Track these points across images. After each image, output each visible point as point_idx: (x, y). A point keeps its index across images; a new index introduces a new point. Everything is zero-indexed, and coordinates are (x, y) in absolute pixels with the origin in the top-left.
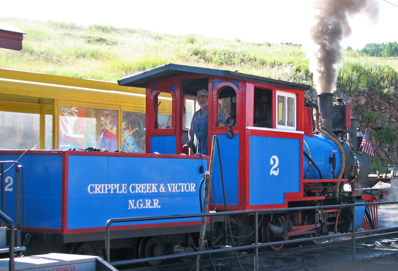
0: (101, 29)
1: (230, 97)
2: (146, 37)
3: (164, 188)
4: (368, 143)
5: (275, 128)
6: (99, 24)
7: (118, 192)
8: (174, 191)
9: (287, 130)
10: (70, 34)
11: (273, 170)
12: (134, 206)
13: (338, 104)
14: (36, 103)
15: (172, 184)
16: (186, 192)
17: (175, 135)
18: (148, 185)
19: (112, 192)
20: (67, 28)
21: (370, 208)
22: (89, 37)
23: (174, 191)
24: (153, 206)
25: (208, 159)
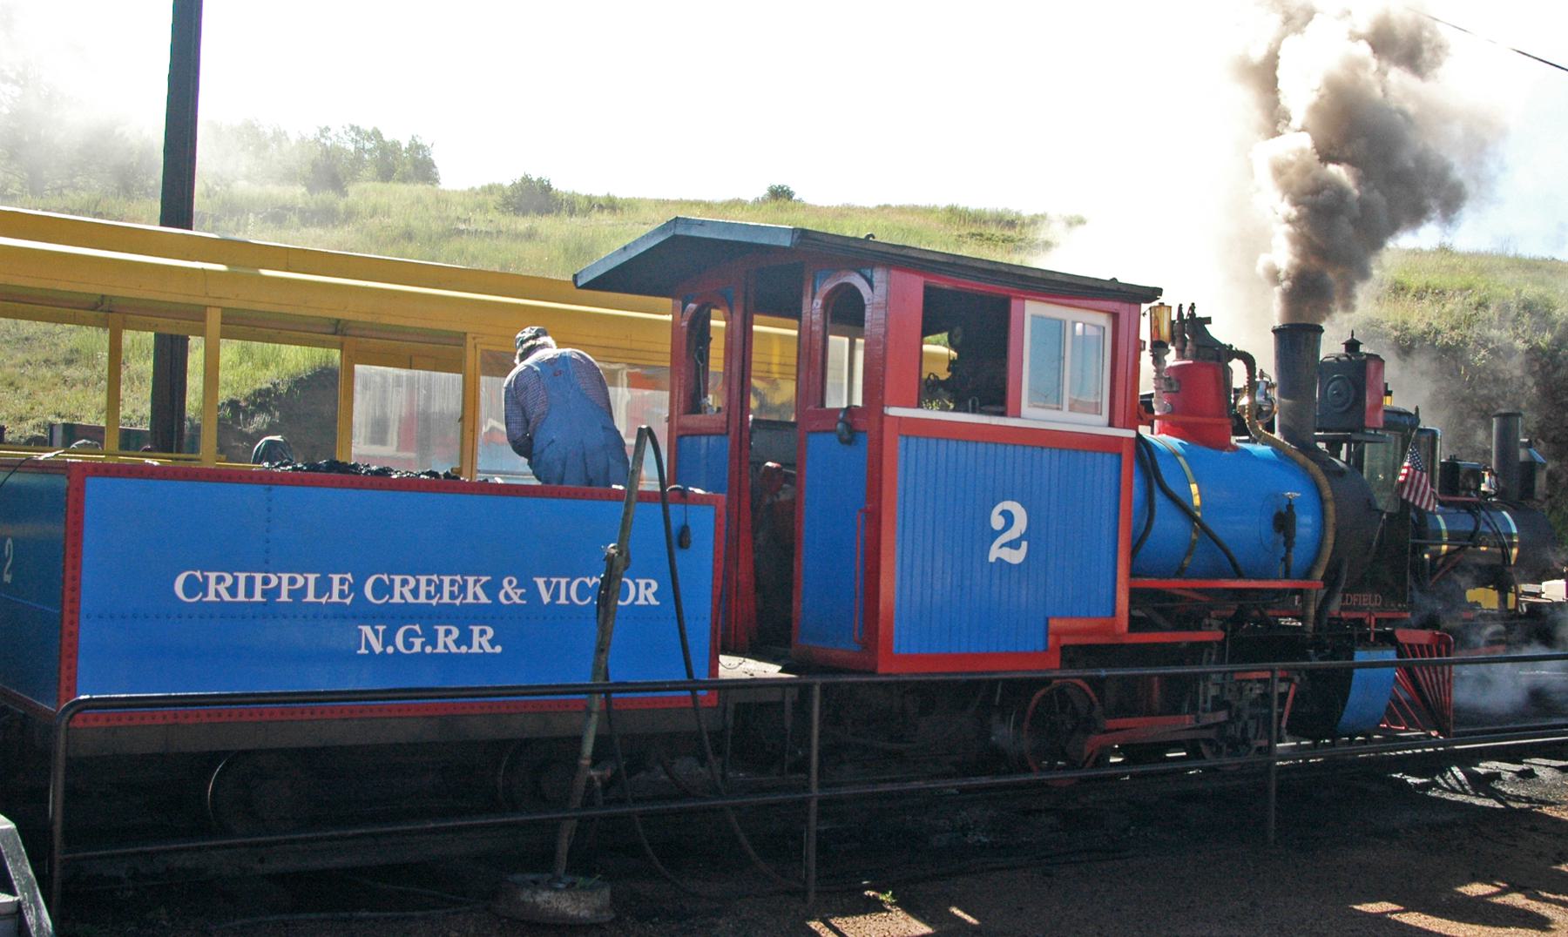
1: (946, 330)
3: (519, 591)
4: (1418, 473)
5: (1018, 415)
7: (310, 597)
10: (981, 235)
12: (385, 646)
14: (85, 309)
15: (554, 580)
16: (576, 605)
17: (727, 433)
18: (447, 580)
19: (284, 597)
20: (985, 222)
23: (563, 600)
24: (470, 647)
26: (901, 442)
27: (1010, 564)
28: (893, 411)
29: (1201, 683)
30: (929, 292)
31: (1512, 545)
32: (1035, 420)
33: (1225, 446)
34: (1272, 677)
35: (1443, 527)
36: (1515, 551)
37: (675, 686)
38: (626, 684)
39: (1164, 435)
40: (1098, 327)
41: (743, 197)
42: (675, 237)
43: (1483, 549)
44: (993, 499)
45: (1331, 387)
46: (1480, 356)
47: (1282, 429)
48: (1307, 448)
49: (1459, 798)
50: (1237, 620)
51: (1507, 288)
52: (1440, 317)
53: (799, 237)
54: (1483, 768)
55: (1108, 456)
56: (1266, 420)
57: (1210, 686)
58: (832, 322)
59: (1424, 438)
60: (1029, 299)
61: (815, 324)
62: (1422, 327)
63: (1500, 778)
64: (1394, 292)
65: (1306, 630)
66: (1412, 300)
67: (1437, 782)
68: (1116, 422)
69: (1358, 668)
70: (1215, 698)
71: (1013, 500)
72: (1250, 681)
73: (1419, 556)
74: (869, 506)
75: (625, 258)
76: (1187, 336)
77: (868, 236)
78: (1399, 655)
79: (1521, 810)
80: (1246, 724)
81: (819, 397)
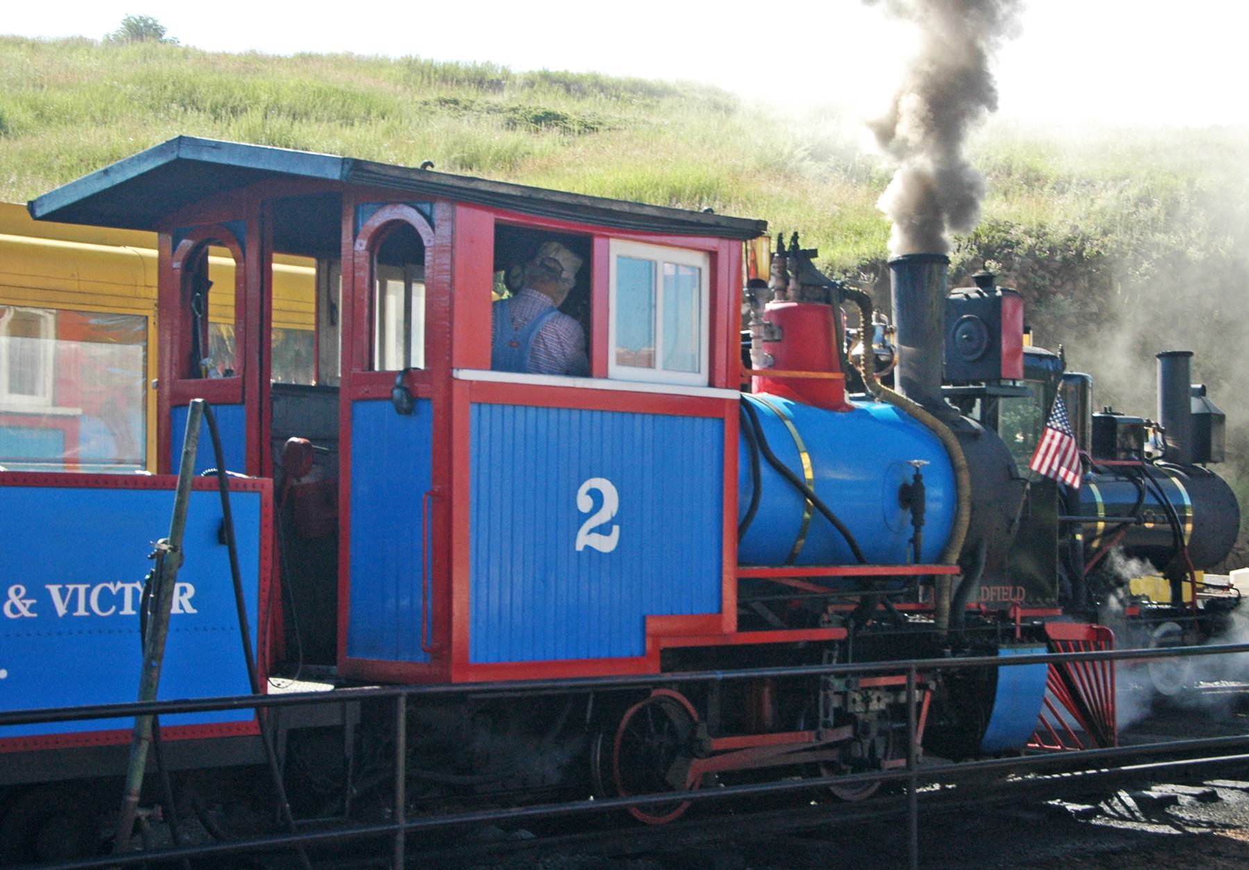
0: (562, 85)
2: (698, 108)
3: (29, 602)
5: (605, 376)
6: (556, 67)
8: (81, 611)
9: (688, 386)
10: (456, 102)
11: (591, 531)
13: (977, 295)
15: (71, 587)
16: (98, 616)
17: (243, 402)
20: (458, 82)
21: (1089, 665)
22: (514, 110)
23: (81, 611)
25: (261, 492)
26: (474, 409)
27: (600, 553)
28: (464, 374)
29: (822, 693)
30: (500, 229)
31: (1185, 520)
32: (628, 381)
33: (839, 406)
34: (909, 683)
35: (1099, 499)
36: (1189, 527)
37: (241, 704)
38: (186, 701)
39: (765, 394)
40: (692, 268)
41: (89, 35)
42: (179, 161)
43: (1149, 525)
44: (579, 477)
45: (960, 330)
46: (1142, 270)
47: (905, 383)
48: (933, 406)
49: (1129, 825)
50: (859, 616)
51: (1176, 177)
52: (1088, 217)
53: (351, 169)
54: (1156, 792)
55: (709, 422)
56: (885, 373)
57: (831, 696)
58: (379, 262)
59: (1071, 387)
60: (613, 237)
61: (361, 269)
62: (1065, 231)
63: (1177, 804)
64: (1027, 183)
65: (941, 626)
66: (1050, 195)
67: (1101, 809)
68: (717, 381)
69: (1004, 664)
70: (837, 711)
71: (601, 477)
72: (877, 688)
73: (1070, 537)
74: (437, 488)
75: (106, 184)
76: (789, 272)
77: (425, 165)
78: (1051, 650)
79: (1201, 834)
80: (873, 742)
81: (366, 357)
